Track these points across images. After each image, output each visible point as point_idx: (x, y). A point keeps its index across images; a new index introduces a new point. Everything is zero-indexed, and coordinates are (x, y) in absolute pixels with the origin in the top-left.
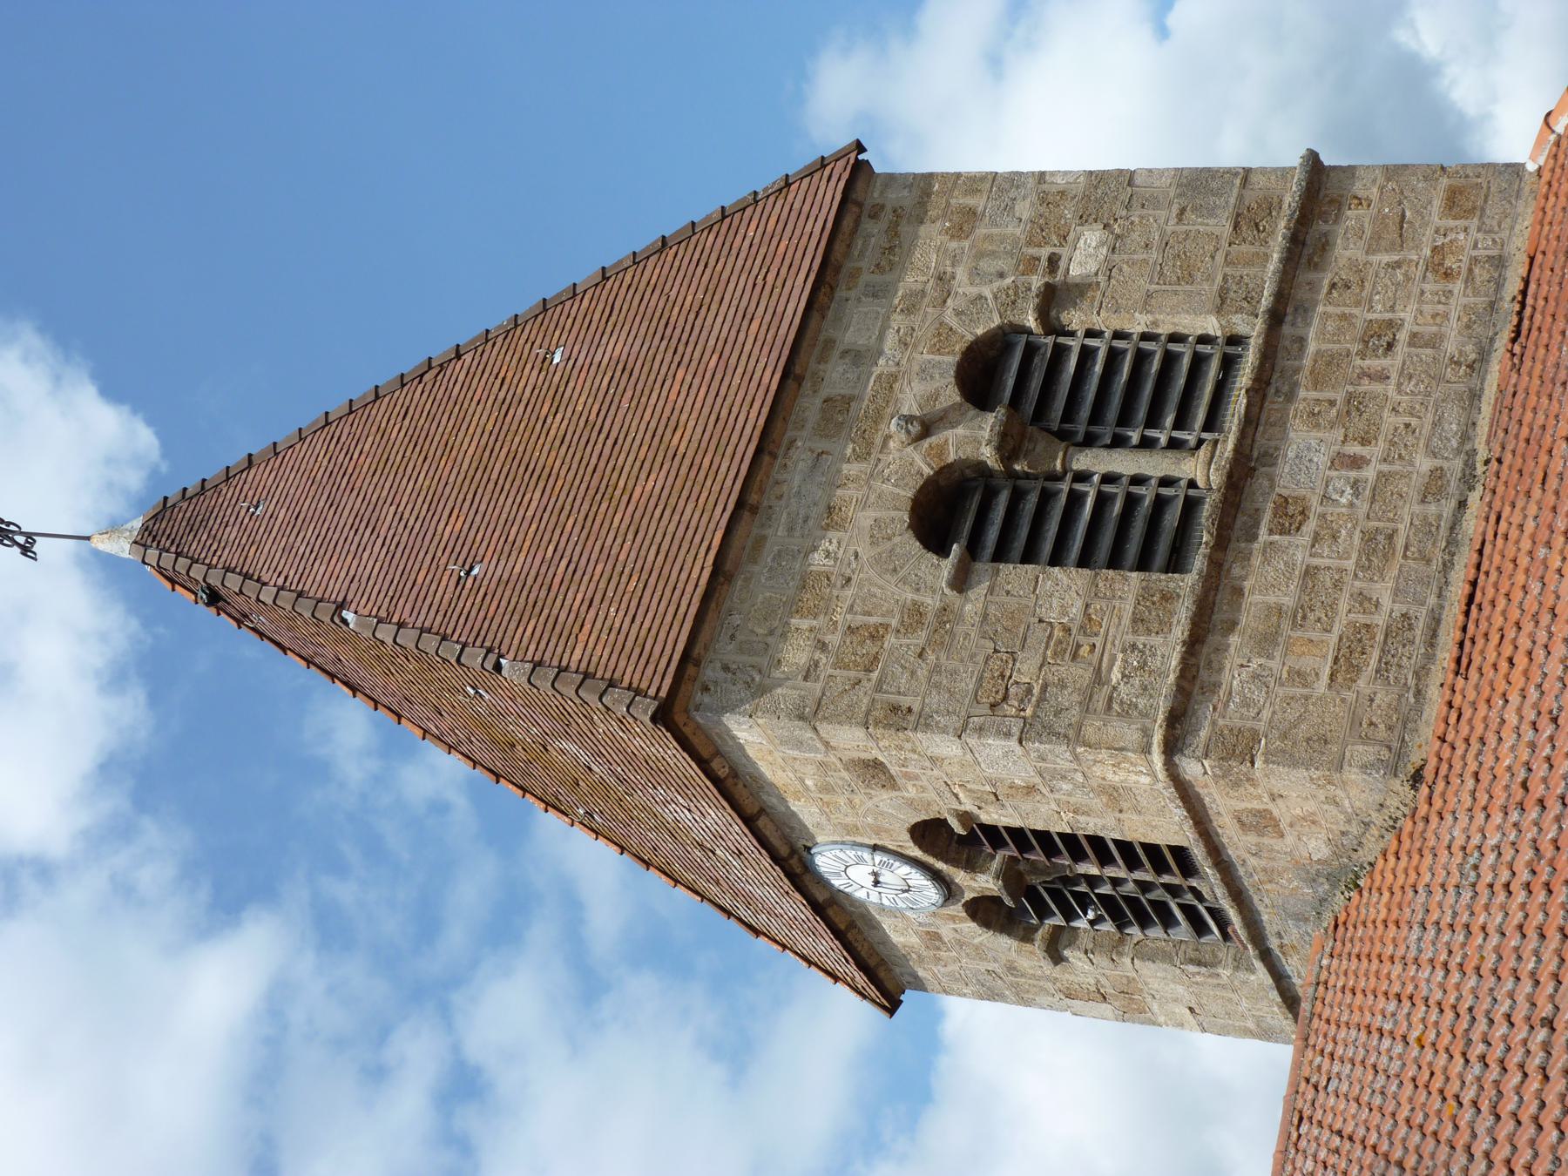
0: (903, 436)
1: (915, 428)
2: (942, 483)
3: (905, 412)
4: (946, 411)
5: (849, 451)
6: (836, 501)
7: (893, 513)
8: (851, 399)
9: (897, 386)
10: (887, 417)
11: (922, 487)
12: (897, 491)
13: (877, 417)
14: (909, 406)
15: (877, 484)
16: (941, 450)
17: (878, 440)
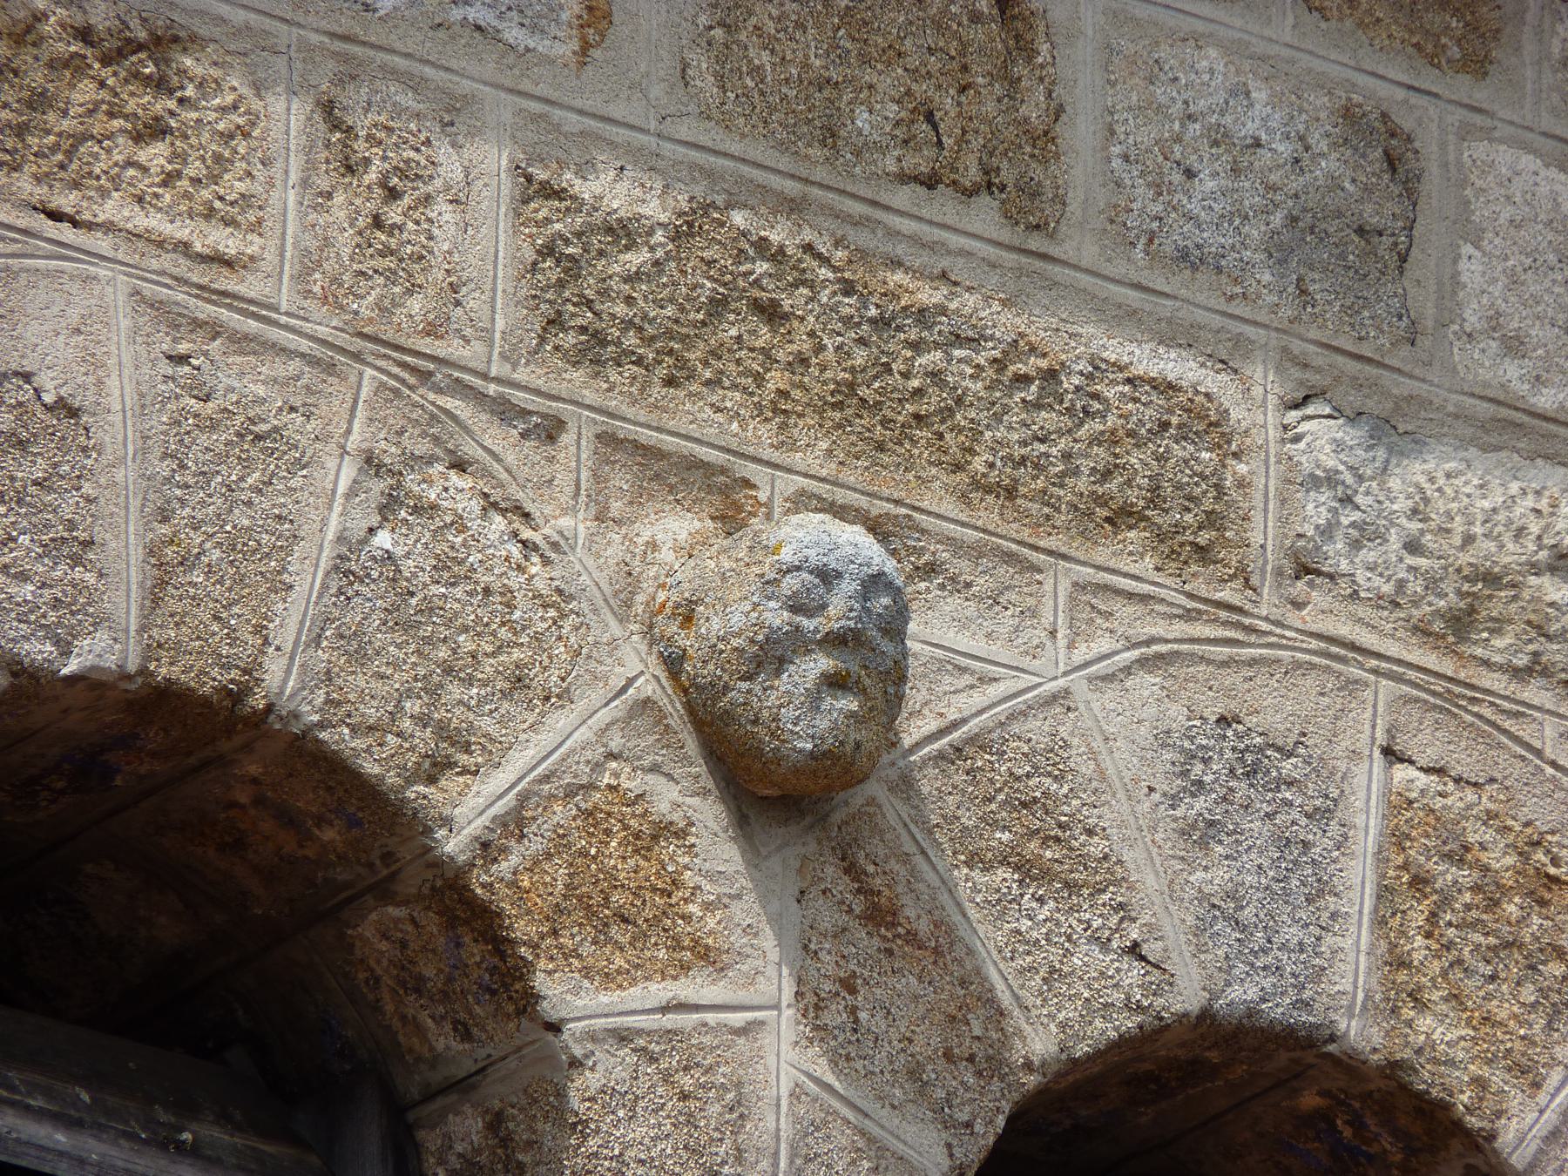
0: (734, 618)
1: (799, 711)
2: (376, 931)
3: (935, 627)
4: (940, 948)
5: (610, 190)
6: (214, 88)
7: (125, 548)
8: (1030, 209)
9: (1130, 558)
10: (887, 489)
11: (335, 773)
12: (308, 573)
13: (876, 412)
14: (978, 661)
15: (354, 419)
16: (640, 918)
17: (698, 422)
